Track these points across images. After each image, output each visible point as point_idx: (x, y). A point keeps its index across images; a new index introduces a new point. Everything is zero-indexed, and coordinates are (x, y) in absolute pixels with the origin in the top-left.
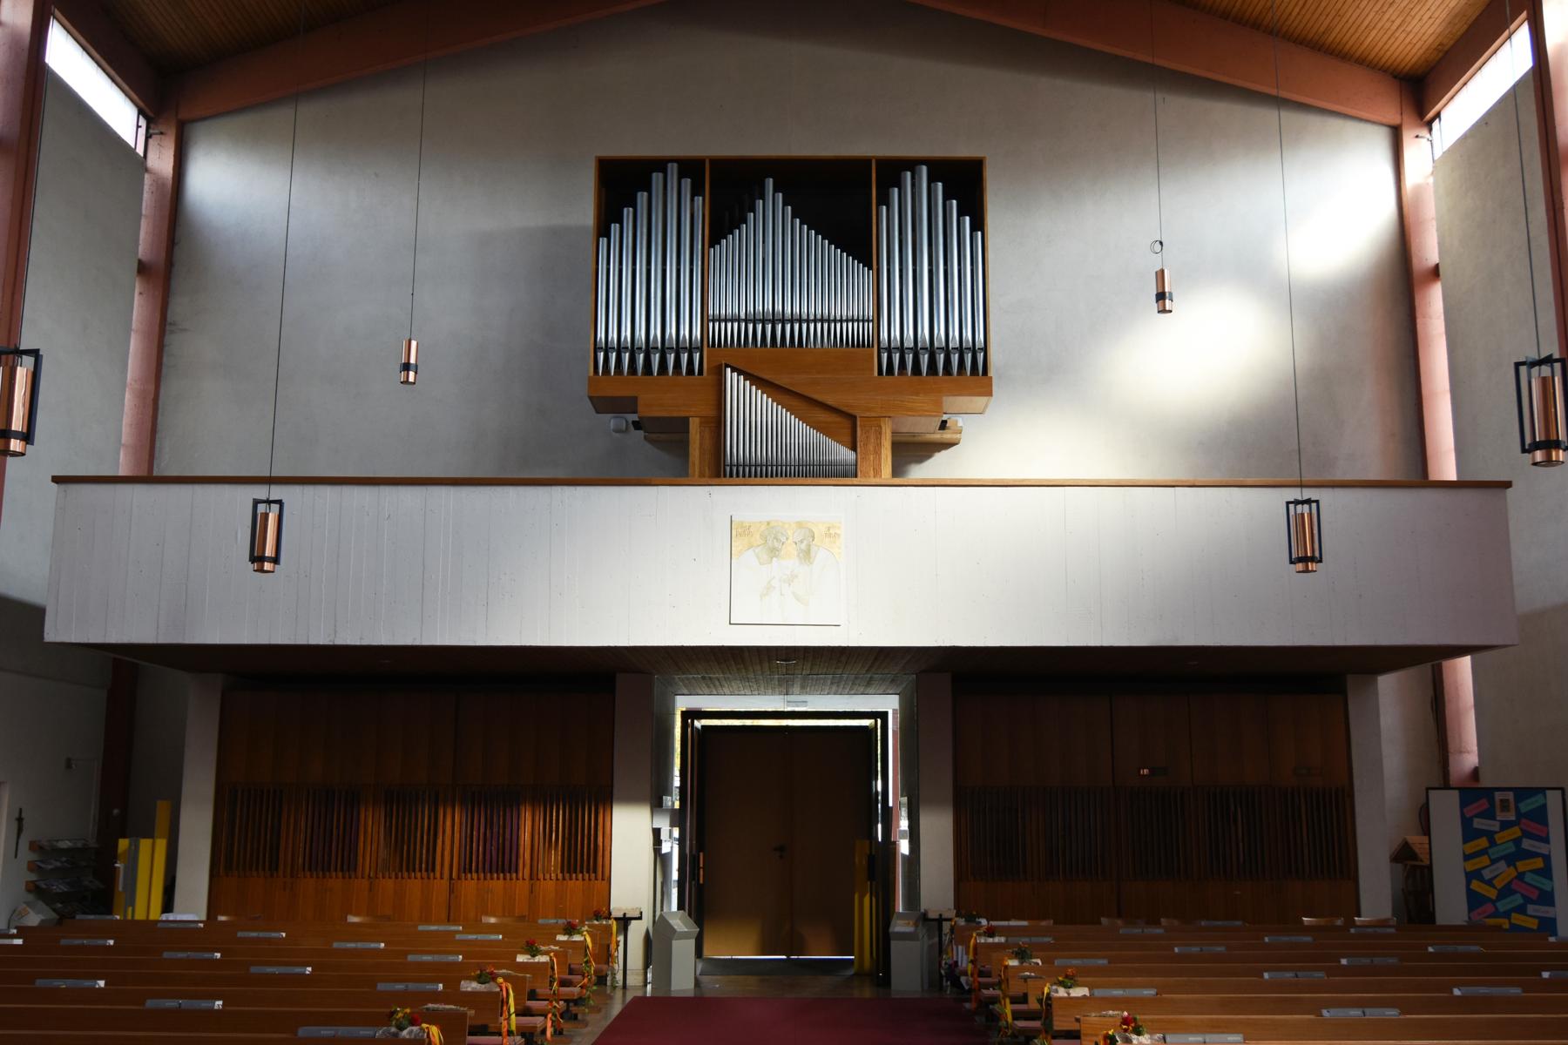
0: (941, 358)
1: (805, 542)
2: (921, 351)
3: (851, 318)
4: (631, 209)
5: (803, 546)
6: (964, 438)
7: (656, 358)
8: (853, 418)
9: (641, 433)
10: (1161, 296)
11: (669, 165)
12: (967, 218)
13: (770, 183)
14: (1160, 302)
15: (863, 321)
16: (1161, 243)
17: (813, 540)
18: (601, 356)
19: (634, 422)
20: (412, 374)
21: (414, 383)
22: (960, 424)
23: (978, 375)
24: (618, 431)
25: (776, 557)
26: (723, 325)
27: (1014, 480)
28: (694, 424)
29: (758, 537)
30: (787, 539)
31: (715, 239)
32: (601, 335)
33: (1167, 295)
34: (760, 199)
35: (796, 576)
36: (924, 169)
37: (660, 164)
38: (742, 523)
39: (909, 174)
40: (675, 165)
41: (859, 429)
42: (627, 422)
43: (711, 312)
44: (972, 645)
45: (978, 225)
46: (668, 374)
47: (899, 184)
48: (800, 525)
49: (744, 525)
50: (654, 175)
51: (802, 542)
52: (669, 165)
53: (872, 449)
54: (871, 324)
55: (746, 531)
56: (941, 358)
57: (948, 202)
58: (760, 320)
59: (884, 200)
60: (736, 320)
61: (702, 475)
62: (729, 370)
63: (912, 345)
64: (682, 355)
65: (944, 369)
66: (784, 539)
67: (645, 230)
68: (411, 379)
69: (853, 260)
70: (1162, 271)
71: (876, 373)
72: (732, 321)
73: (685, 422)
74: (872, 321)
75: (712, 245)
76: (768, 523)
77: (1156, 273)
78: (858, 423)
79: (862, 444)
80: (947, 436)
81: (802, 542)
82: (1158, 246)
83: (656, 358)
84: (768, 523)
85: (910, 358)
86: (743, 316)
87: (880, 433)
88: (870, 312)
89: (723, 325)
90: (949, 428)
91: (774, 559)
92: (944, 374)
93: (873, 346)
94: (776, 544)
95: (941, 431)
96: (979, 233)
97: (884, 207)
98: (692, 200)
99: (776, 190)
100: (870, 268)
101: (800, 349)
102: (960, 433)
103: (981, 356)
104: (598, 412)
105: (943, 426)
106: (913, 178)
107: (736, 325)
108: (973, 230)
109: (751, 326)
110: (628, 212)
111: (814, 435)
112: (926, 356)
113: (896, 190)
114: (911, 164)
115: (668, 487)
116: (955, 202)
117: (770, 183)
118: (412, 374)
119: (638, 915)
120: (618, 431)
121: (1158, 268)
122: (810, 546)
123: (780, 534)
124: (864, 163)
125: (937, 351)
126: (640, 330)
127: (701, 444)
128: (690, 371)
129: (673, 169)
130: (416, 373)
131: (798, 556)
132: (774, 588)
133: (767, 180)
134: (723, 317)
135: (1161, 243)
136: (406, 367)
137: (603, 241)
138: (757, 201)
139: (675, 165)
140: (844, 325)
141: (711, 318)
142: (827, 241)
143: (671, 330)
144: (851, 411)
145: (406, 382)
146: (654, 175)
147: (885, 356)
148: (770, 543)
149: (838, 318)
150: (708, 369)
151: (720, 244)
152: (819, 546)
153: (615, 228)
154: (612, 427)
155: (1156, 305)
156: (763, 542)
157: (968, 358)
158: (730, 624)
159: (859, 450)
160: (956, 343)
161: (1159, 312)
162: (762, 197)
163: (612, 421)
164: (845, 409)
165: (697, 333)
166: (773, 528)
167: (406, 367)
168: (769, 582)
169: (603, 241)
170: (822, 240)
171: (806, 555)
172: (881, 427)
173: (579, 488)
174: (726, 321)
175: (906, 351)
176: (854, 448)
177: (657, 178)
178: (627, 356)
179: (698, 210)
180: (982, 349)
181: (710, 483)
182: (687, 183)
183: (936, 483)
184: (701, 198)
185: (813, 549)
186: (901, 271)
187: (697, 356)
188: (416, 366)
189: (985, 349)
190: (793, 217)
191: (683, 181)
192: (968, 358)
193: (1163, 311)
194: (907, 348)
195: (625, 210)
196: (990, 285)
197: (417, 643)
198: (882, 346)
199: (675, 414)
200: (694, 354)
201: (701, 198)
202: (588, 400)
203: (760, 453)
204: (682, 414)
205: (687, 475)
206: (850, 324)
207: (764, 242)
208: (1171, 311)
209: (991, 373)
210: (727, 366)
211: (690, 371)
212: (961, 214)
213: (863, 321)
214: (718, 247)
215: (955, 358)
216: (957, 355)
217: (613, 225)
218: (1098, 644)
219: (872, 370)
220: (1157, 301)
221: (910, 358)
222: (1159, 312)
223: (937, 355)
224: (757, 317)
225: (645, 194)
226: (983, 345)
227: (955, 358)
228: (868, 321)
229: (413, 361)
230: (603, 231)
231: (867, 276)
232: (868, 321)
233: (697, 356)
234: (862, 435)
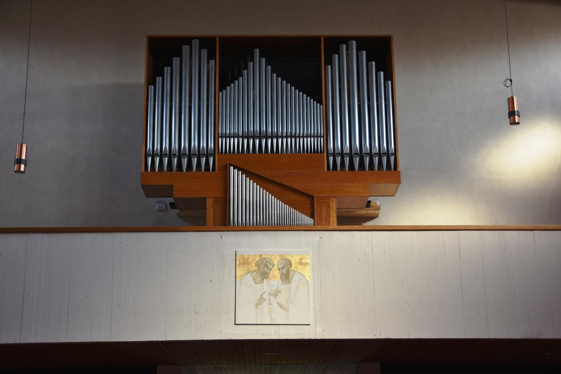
0: (367, 159)
1: (285, 269)
2: (354, 155)
3: (309, 135)
4: (169, 68)
5: (284, 271)
6: (381, 213)
7: (185, 161)
8: (312, 197)
9: (176, 211)
10: (512, 114)
11: (194, 41)
12: (382, 73)
13: (257, 51)
14: (512, 117)
15: (317, 137)
16: (511, 80)
17: (291, 267)
18: (150, 159)
19: (170, 203)
20: (23, 166)
21: (24, 172)
22: (378, 204)
23: (391, 170)
24: (159, 211)
25: (266, 278)
26: (228, 140)
27: (425, 226)
28: (209, 202)
29: (254, 265)
30: (273, 266)
31: (222, 87)
32: (149, 146)
33: (516, 112)
34: (251, 61)
35: (280, 292)
36: (354, 43)
37: (188, 41)
38: (243, 256)
39: (344, 46)
40: (197, 41)
41: (315, 204)
42: (166, 205)
43: (220, 132)
44: (399, 338)
45: (389, 77)
46: (192, 170)
47: (338, 52)
48: (282, 258)
49: (244, 257)
50: (184, 47)
51: (283, 268)
52: (194, 41)
53: (324, 217)
54: (322, 139)
55: (246, 262)
56: (367, 159)
57: (369, 63)
58: (252, 136)
59: (329, 62)
60: (236, 137)
61: (214, 224)
62: (232, 168)
63: (349, 151)
64: (202, 159)
65: (369, 167)
66: (271, 267)
67: (178, 94)
68: (22, 169)
69: (310, 99)
70: (512, 98)
71: (326, 170)
72: (234, 137)
73: (203, 201)
74: (323, 137)
75: (221, 90)
76: (261, 256)
77: (508, 99)
78: (315, 200)
79: (318, 214)
80: (370, 212)
81: (283, 268)
82: (508, 83)
83: (185, 161)
84: (261, 256)
85: (347, 160)
86: (241, 134)
87: (329, 207)
88: (321, 131)
89: (228, 140)
90: (372, 206)
91: (265, 280)
92: (369, 170)
93: (323, 153)
94: (266, 270)
95: (367, 208)
96: (390, 82)
97: (329, 67)
98: (208, 63)
99: (261, 56)
100: (321, 104)
101: (277, 154)
102: (379, 210)
103: (392, 159)
104: (147, 197)
105: (368, 204)
106: (347, 50)
107: (236, 140)
108: (386, 80)
109: (246, 141)
110: (167, 70)
111: (287, 209)
112: (358, 159)
113: (337, 56)
114: (346, 40)
115: (193, 233)
116: (374, 63)
117: (257, 51)
118: (23, 166)
119: (378, 209)
120: (159, 211)
121: (510, 96)
122: (289, 270)
123: (268, 263)
124: (317, 39)
125: (365, 155)
126: (175, 143)
127: (214, 215)
128: (207, 168)
129: (195, 43)
130: (25, 165)
131: (281, 277)
132: (265, 299)
133: (255, 50)
134: (228, 134)
135: (511, 80)
136: (19, 161)
137: (151, 88)
138: (249, 63)
139: (197, 41)
140: (305, 139)
141: (220, 135)
142: (293, 87)
143: (194, 143)
144: (311, 194)
145: (19, 171)
146: (184, 47)
147: (331, 159)
148: (262, 269)
149: (301, 135)
150: (218, 167)
151: (226, 89)
152: (295, 271)
153: (159, 79)
154: (156, 208)
155: (509, 120)
156: (258, 269)
157: (385, 159)
158: (235, 324)
159: (316, 218)
160: (376, 150)
161: (511, 124)
162: (253, 61)
163: (157, 205)
164: (306, 192)
165: (211, 145)
166: (264, 259)
167: (19, 161)
168: (262, 296)
169: (151, 88)
170: (291, 86)
171: (286, 277)
172: (329, 203)
173: (133, 234)
174: (230, 137)
175: (345, 155)
176: (312, 216)
177: (186, 49)
178: (166, 160)
179: (212, 69)
180: (393, 154)
181: (221, 229)
182: (205, 52)
183: (372, 229)
184: (213, 61)
185: (291, 273)
186: (340, 106)
187: (211, 159)
188: (26, 161)
189: (395, 154)
190: (272, 72)
191: (202, 50)
192: (385, 159)
193: (513, 123)
194: (345, 154)
195: (166, 68)
196: (397, 119)
197: (17, 342)
198: (329, 152)
199: (198, 196)
200: (210, 158)
201: (213, 61)
202: (141, 186)
203: (252, 220)
204: (202, 196)
205: (204, 224)
206: (309, 139)
207: (253, 88)
208: (518, 123)
209: (401, 167)
210: (231, 165)
211: (207, 168)
212: (377, 70)
213: (317, 137)
214: (224, 91)
215: (376, 160)
216: (377, 158)
217: (157, 78)
218: (486, 337)
219: (324, 168)
220: (509, 118)
221: (347, 160)
222: (511, 124)
223: (365, 158)
224: (250, 135)
225: (178, 58)
226: (393, 151)
227: (376, 160)
228: (320, 137)
229: (24, 157)
230: (151, 81)
231: (318, 108)
232: (320, 137)
233: (211, 159)
234: (317, 209)
